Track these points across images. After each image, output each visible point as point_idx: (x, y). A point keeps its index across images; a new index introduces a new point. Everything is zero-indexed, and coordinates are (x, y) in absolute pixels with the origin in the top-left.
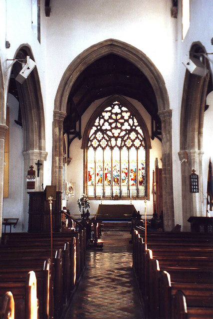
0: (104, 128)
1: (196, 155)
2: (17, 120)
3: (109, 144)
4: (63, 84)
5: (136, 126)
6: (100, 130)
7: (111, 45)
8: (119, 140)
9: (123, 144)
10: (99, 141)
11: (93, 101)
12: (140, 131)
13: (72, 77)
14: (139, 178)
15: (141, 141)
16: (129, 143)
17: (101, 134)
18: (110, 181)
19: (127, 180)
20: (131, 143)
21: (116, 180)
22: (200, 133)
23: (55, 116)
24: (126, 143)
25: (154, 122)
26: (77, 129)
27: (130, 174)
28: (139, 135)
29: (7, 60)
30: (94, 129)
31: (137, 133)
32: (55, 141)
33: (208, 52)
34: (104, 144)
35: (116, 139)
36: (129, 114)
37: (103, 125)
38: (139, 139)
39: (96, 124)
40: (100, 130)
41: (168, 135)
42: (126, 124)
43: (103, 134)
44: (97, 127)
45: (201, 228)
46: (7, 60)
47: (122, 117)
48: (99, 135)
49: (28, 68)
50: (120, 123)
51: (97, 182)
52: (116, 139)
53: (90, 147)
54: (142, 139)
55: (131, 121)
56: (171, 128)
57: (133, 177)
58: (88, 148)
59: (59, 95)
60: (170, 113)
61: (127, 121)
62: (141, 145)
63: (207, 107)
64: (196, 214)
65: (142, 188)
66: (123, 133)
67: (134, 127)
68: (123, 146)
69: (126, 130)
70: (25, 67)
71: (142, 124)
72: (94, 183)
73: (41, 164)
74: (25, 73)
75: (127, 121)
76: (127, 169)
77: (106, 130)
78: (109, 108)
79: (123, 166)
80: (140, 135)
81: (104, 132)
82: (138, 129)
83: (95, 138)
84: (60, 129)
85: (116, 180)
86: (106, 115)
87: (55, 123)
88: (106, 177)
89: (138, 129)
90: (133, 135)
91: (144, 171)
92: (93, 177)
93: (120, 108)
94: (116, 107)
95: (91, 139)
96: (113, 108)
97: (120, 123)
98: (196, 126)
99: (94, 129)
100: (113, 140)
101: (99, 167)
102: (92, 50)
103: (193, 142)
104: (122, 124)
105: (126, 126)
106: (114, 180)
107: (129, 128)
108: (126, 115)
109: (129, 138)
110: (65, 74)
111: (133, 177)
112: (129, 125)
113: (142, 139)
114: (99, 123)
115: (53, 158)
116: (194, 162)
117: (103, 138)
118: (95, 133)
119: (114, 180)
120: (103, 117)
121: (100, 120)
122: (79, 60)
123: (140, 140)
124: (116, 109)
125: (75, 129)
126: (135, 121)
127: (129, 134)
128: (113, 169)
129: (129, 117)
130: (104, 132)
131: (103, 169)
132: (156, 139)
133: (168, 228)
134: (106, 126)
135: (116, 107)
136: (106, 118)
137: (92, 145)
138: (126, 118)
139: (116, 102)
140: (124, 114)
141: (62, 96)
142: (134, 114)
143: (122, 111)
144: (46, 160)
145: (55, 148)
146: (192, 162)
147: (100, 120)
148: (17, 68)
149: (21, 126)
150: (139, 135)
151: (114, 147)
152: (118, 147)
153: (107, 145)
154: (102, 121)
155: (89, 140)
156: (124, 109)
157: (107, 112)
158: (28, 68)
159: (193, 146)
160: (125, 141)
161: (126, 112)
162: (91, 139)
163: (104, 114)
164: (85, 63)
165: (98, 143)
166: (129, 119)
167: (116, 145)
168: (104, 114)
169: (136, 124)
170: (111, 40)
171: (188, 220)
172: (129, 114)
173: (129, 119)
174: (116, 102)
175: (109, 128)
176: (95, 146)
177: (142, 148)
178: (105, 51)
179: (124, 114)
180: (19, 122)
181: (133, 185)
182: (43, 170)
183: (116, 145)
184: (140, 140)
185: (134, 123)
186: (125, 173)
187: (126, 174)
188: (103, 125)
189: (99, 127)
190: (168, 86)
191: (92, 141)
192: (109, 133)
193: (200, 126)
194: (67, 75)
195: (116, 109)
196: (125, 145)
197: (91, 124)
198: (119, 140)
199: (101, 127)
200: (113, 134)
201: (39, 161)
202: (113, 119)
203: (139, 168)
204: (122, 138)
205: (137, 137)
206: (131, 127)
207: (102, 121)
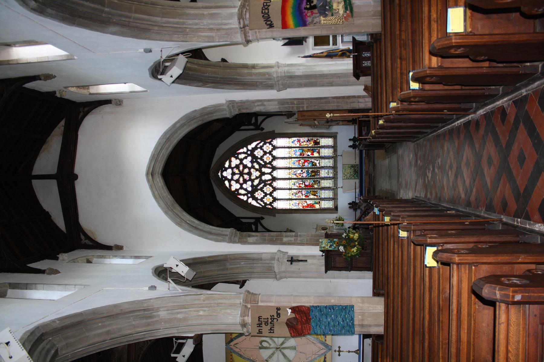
0: (250, 189)
1: (280, 70)
2: (239, 286)
3: (269, 182)
4: (197, 232)
5: (248, 150)
6: (252, 194)
7: (152, 175)
8: (264, 170)
9: (269, 166)
10: (266, 194)
11: (218, 201)
12: (253, 145)
13: (189, 221)
14: (310, 145)
15: (265, 144)
16: (267, 158)
17: (257, 193)
18: (314, 181)
19: (313, 160)
20: (268, 155)
21: (313, 174)
22: (254, 67)
23: (234, 242)
24: (268, 162)
25: (243, 128)
26: (252, 221)
27: (305, 156)
28: (259, 146)
29: (169, 289)
30: (250, 200)
31: (256, 148)
32: (264, 242)
33: (159, 58)
34: (268, 189)
35: (263, 174)
36: (233, 159)
37: (246, 190)
38: (263, 146)
39: (245, 198)
40: (252, 194)
41: (256, 104)
42: (249, 183)
43: (257, 190)
44: (248, 198)
45: (366, 65)
46: (169, 289)
47: (237, 167)
48: (259, 195)
49: (172, 76)
50: (243, 170)
51: (315, 197)
52: (263, 174)
53: (272, 206)
54: (263, 143)
55: (242, 156)
56: (247, 101)
57: (309, 153)
58: (274, 209)
59: (211, 236)
60: (232, 103)
61: (241, 160)
62: (270, 143)
63: (224, 60)
64: (350, 70)
65: (324, 142)
66: (257, 166)
67: (249, 152)
68: (272, 165)
69: (252, 162)
70: (175, 269)
71: (245, 143)
72: (317, 201)
73: (292, 258)
74: (183, 270)
75: (241, 160)
76: (300, 160)
77: (252, 186)
78: (227, 183)
79: (296, 165)
80: (258, 144)
81: (255, 189)
82: (250, 147)
83: (262, 200)
84: (249, 236)
85: (313, 174)
86: (235, 186)
87: (242, 241)
88: (309, 186)
89: (250, 147)
90: (258, 153)
91: (302, 139)
92: (309, 202)
93: (226, 169)
94: (225, 174)
95: (263, 205)
96: (226, 178)
97: (243, 170)
98: (246, 71)
99: (250, 200)
100: (264, 178)
101: (297, 196)
102: (158, 197)
103: (263, 74)
104: (245, 167)
105: (247, 162)
106: (313, 176)
107: (250, 158)
108: (235, 162)
109: (261, 158)
110: (185, 229)
111: (309, 153)
112: (246, 158)
113: (263, 143)
114: (244, 195)
115: (285, 244)
116: (288, 72)
117: (261, 189)
118: (256, 199)
119: (313, 176)
120: (237, 190)
121: (241, 194)
122: (170, 213)
123: (264, 144)
124: (227, 174)
125: (251, 223)
126: (241, 151)
127: (257, 158)
128: (300, 177)
129: (237, 158)
130: (255, 189)
131: (300, 189)
132: (263, 126)
133: (368, 103)
134: (248, 186)
135: (225, 174)
136: (238, 186)
137: (270, 204)
138: (238, 162)
139: (219, 174)
140: (233, 165)
141: (210, 233)
142: (233, 152)
143: (230, 167)
144: (287, 253)
145: (272, 242)
146: (288, 75)
147: (241, 194)
148: (178, 279)
149: (246, 280)
150: (259, 146)
151: (272, 176)
152: (272, 172)
153: (270, 185)
154: (242, 192)
155: (264, 208)
156: (227, 165)
157: (230, 185)
158: (172, 76)
159: (269, 74)
160: (265, 162)
161: (230, 162)
162: (263, 205)
163: (233, 189)
164: (173, 205)
165: (268, 196)
166: (239, 159)
167: (270, 174)
168: (233, 189)
169: (245, 150)
170: (147, 174)
171: (358, 80)
172: (233, 159)
173: (239, 159)
174: (219, 174)
175: (249, 183)
176: (271, 199)
177: (275, 142)
178: (159, 181)
179: (233, 165)
180: (242, 284)
181: (319, 153)
182: (299, 256)
183: (270, 174)
184: (264, 144)
185: (244, 153)
186: (304, 163)
187: (305, 161)
188: (246, 190)
189: (249, 195)
190: (198, 106)
191: (266, 204)
192: (256, 182)
193: (245, 66)
194: (186, 226)
195: (227, 174)
196: (270, 163)
197: (245, 205)
198: (264, 170)
199: (249, 192)
200: (257, 178)
201: (288, 261)
202: (239, 177)
203: (298, 145)
204: (261, 166)
205: (261, 148)
206: (249, 155)
207: (242, 192)
